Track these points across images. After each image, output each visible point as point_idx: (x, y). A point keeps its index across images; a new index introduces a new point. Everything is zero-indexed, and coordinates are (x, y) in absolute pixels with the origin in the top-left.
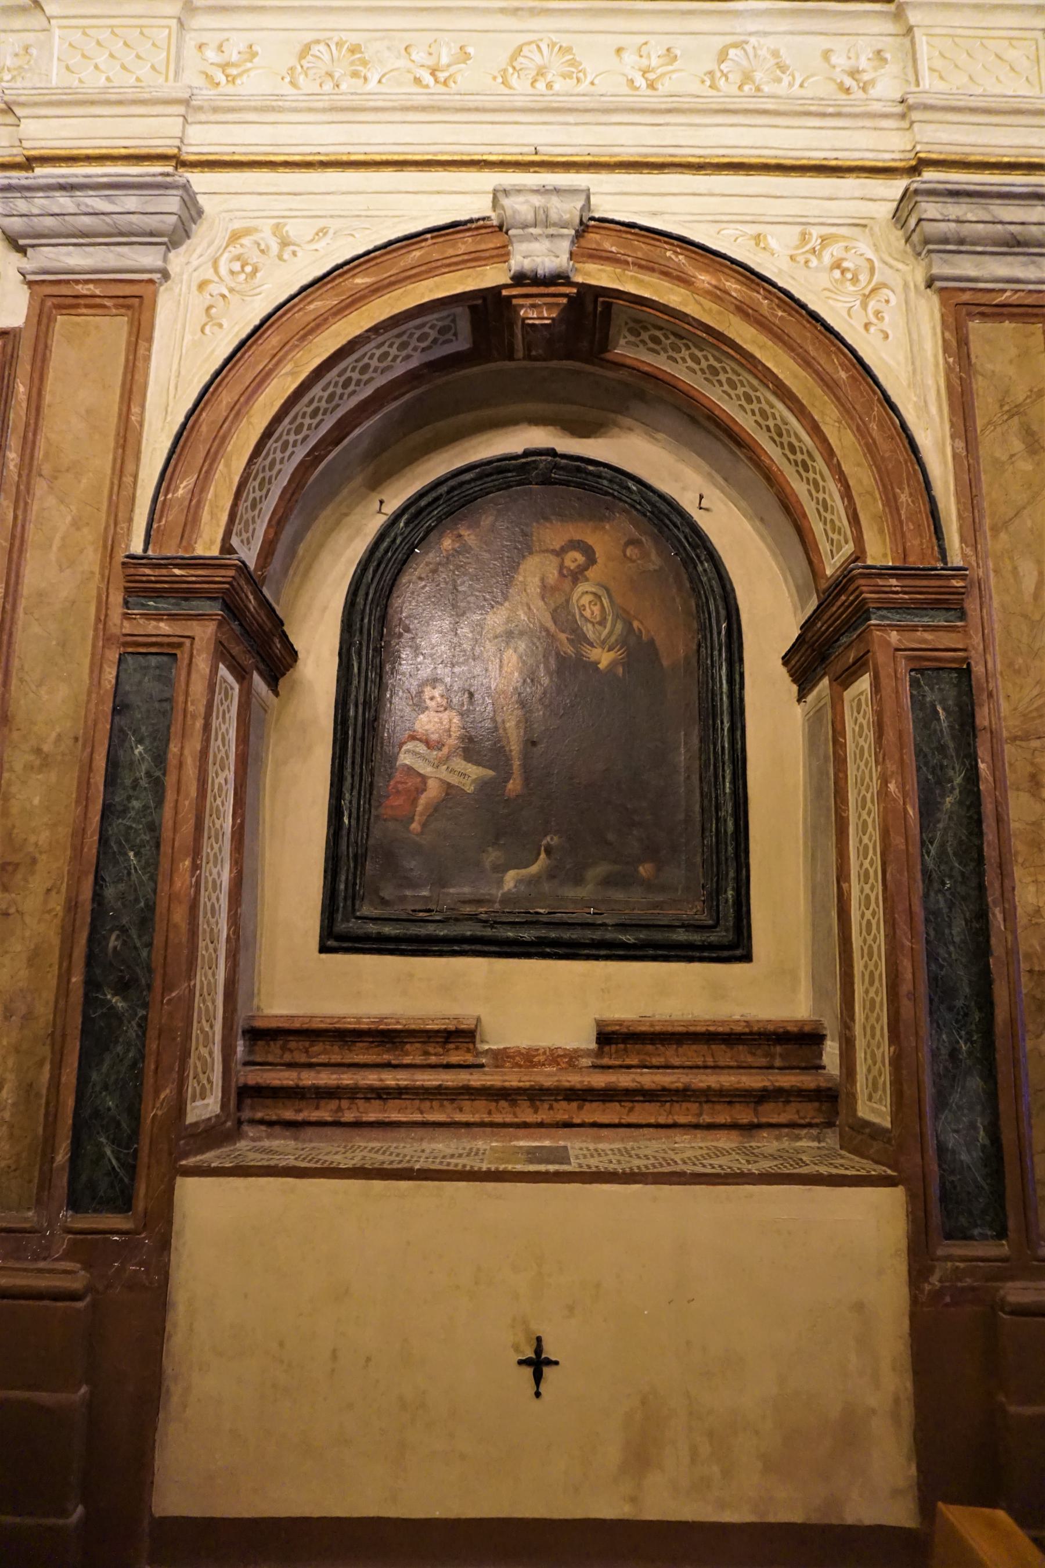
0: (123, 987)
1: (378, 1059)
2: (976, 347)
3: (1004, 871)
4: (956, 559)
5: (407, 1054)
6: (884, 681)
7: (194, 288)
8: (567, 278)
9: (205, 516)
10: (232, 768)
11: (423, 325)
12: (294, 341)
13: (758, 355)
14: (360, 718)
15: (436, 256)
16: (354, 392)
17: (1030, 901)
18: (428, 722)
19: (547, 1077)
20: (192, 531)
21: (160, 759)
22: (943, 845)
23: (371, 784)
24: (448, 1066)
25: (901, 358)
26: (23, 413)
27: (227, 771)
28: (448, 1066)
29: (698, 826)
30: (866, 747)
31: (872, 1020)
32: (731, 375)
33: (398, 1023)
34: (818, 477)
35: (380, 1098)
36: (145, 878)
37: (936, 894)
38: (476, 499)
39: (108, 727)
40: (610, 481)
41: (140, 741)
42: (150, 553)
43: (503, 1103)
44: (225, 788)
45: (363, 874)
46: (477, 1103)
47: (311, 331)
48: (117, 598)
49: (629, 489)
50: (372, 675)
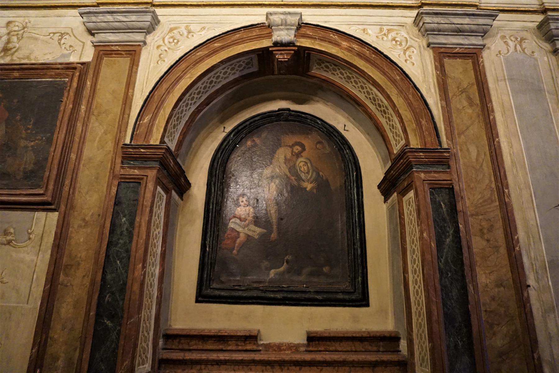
0: (112, 317)
1: (218, 348)
2: (447, 68)
3: (472, 270)
4: (445, 146)
5: (229, 345)
6: (419, 193)
7: (155, 48)
8: (294, 43)
9: (155, 129)
10: (162, 227)
11: (240, 61)
12: (191, 66)
13: (366, 71)
14: (214, 209)
15: (245, 36)
16: (214, 86)
17: (483, 281)
18: (241, 211)
19: (287, 356)
20: (149, 135)
21: (132, 223)
22: (446, 258)
23: (218, 235)
24: (246, 351)
25: (419, 72)
26: (88, 92)
27: (159, 229)
28: (246, 351)
29: (347, 252)
30: (413, 219)
31: (421, 331)
32: (355, 79)
33: (226, 332)
34: (390, 116)
35: (218, 364)
36: (123, 271)
37: (445, 278)
38: (260, 126)
39: (112, 210)
40: (311, 120)
41: (124, 216)
42: (132, 143)
43: (268, 367)
44: (158, 236)
45: (214, 271)
46: (258, 367)
47: (197, 63)
48: (119, 161)
49: (318, 123)
50: (219, 193)
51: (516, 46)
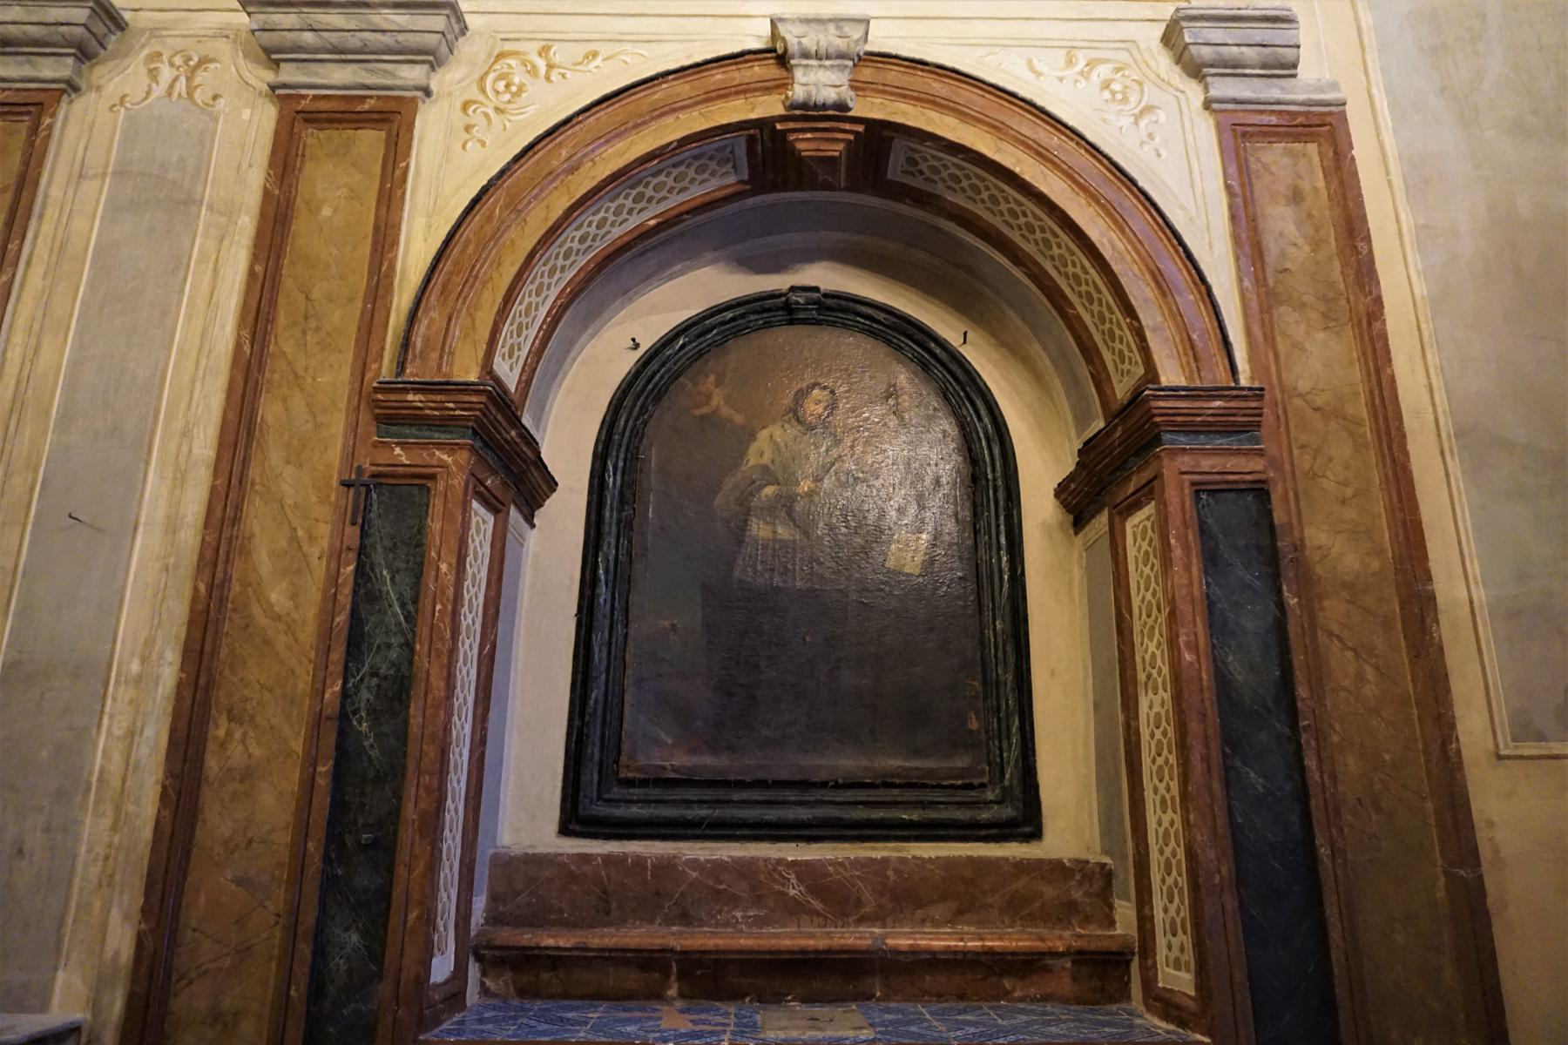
51: (176, 79)
